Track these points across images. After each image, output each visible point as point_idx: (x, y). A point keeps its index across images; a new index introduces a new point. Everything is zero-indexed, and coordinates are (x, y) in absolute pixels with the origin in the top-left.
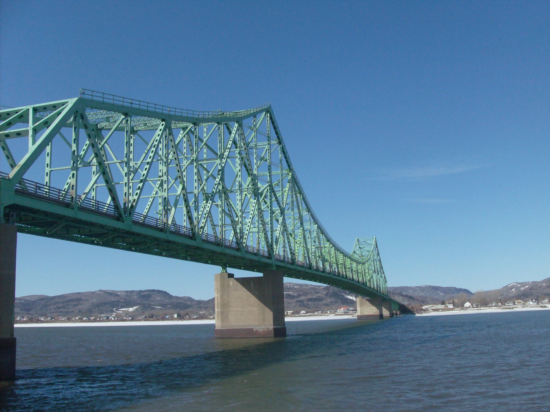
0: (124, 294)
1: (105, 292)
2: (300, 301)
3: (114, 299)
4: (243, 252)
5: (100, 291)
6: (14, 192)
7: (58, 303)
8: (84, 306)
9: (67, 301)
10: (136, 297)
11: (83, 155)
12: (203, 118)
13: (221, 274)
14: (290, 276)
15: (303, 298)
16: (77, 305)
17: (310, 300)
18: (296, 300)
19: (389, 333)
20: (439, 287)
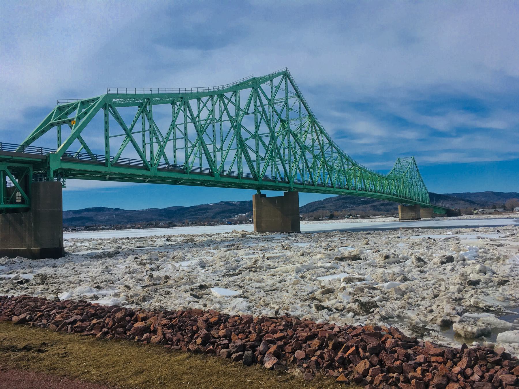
0: (239, 203)
1: (225, 202)
2: (374, 206)
3: (231, 207)
4: (260, 181)
5: (221, 202)
6: (60, 161)
7: (191, 211)
8: (210, 214)
9: (198, 210)
10: (247, 206)
11: (100, 100)
12: (144, 94)
13: (256, 195)
14: (77, 228)
15: (376, 204)
16: (205, 213)
17: (382, 205)
18: (370, 205)
19: (341, 231)
20: (501, 193)
